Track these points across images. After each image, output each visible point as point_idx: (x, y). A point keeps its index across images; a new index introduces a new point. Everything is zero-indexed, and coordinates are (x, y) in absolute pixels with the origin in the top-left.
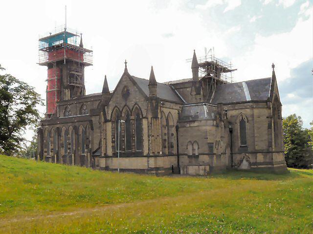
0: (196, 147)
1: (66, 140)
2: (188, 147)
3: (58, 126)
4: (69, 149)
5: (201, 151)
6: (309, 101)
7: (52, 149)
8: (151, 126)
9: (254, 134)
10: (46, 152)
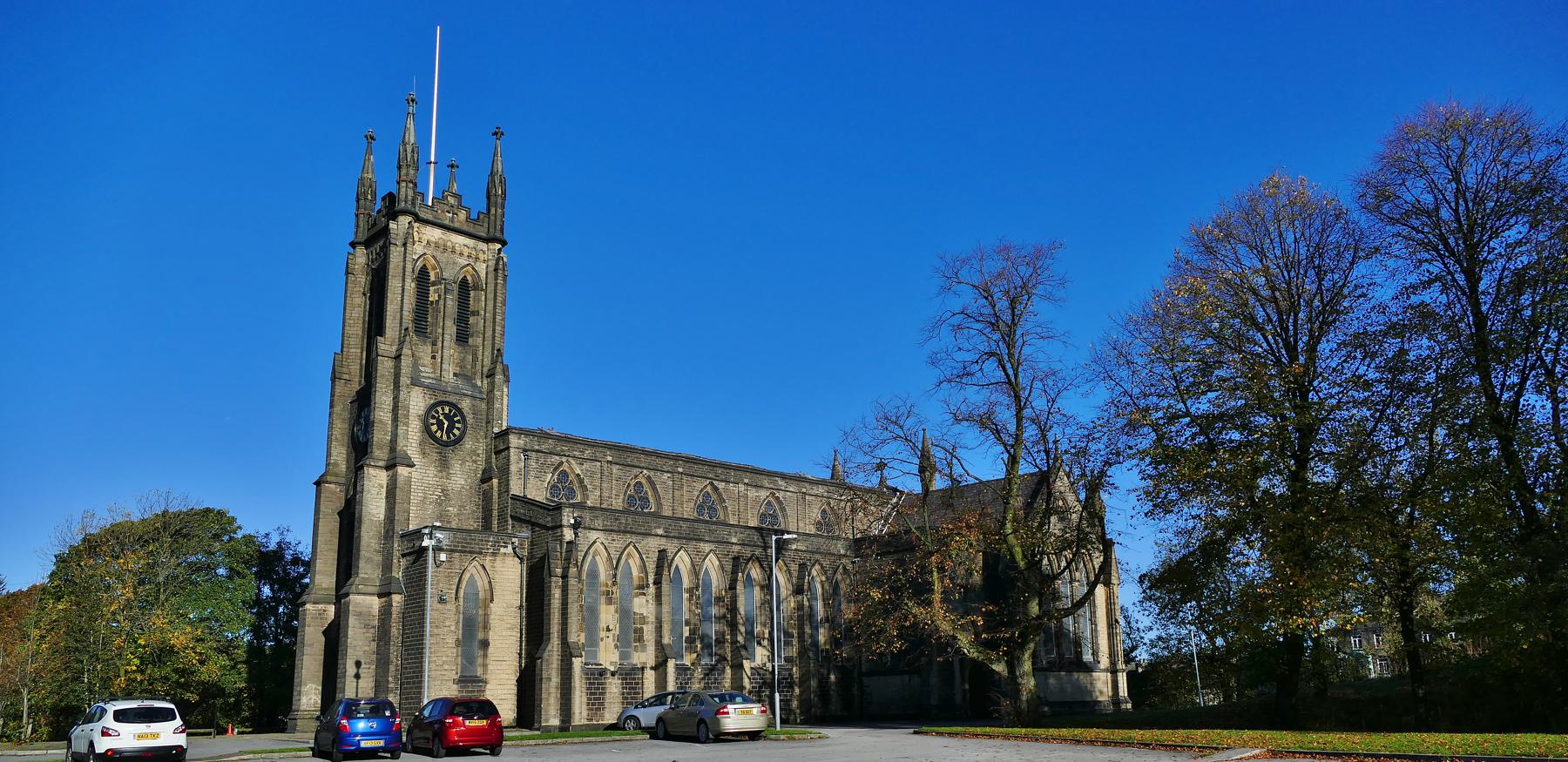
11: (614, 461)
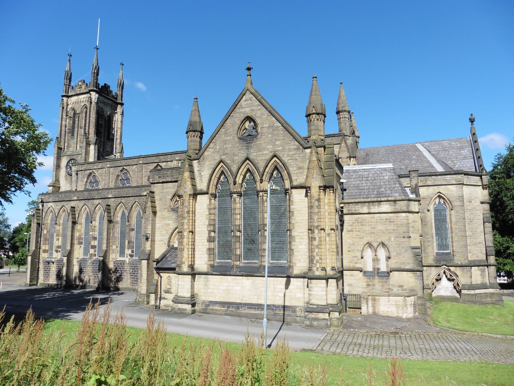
0: (382, 253)
1: (87, 233)
2: (364, 254)
3: (73, 204)
4: (94, 247)
5: (393, 263)
6: (1, 235)
7: (59, 247)
8: (319, 207)
9: (465, 231)
10: (45, 251)
11: (111, 166)
